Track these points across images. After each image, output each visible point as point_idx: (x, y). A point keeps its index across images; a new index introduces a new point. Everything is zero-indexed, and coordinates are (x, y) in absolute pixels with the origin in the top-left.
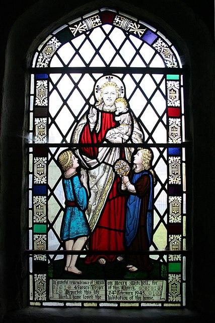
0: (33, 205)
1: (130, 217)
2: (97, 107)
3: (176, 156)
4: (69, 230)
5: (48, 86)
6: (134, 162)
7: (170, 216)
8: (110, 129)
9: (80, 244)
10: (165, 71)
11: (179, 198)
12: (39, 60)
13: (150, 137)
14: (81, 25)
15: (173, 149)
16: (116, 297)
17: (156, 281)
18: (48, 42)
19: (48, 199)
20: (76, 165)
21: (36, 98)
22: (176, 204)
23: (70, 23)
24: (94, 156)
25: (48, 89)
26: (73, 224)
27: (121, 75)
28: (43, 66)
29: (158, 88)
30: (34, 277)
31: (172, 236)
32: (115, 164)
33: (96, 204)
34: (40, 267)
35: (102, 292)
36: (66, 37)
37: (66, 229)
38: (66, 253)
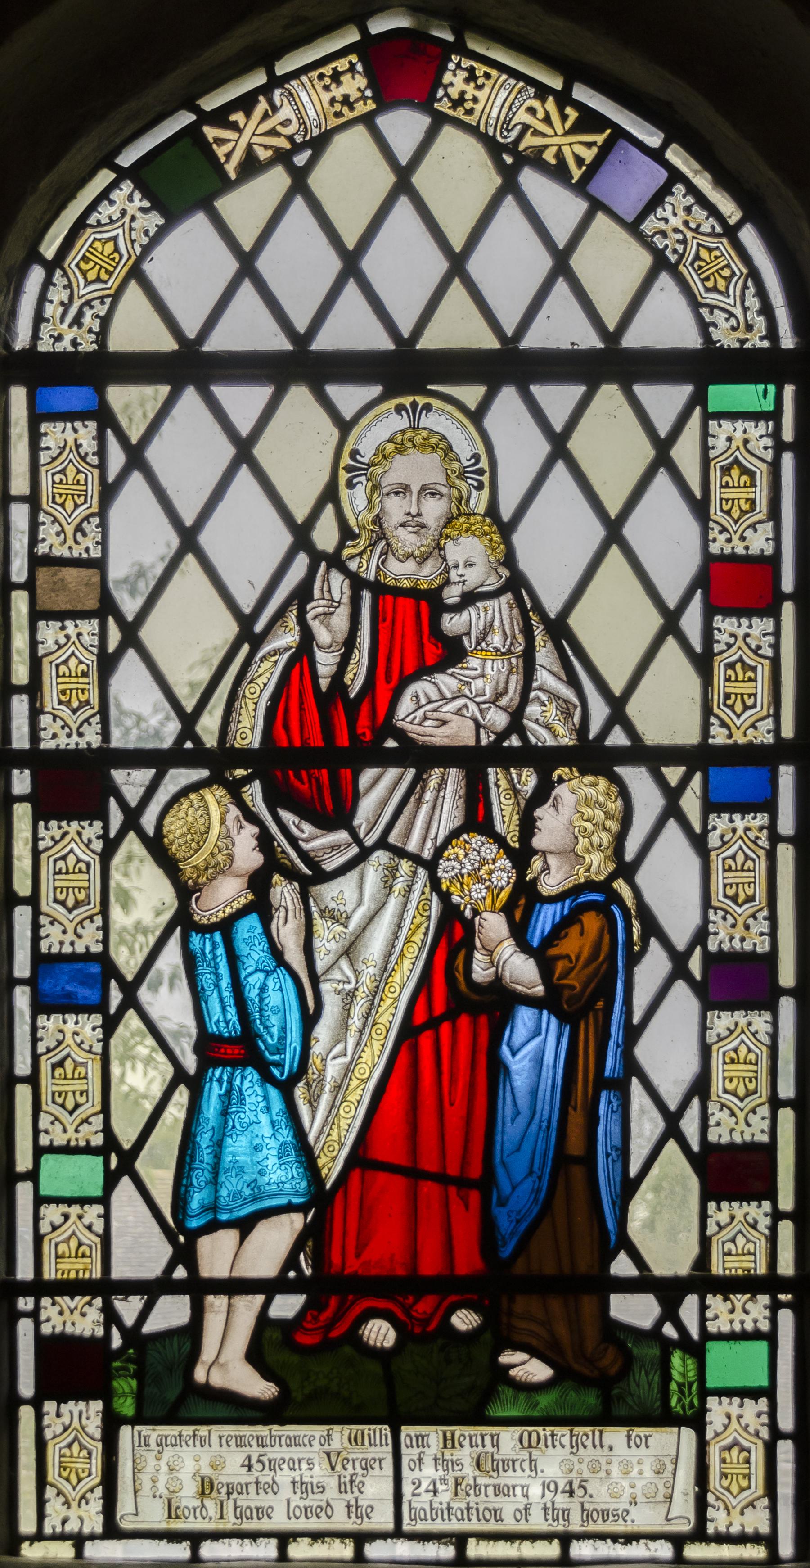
0: (36, 1058)
1: (518, 1113)
2: (353, 566)
3: (745, 808)
4: (215, 1182)
5: (101, 452)
6: (537, 842)
7: (713, 1107)
8: (416, 677)
9: (270, 1247)
10: (705, 366)
11: (760, 1022)
12: (49, 310)
13: (618, 715)
14: (266, 116)
15: (726, 772)
16: (449, 1509)
17: (642, 1431)
18: (92, 207)
19: (110, 1026)
20: (247, 855)
21: (42, 517)
22: (743, 1050)
23: (211, 103)
24: (336, 813)
25: (102, 466)
26: (237, 1147)
27: (471, 394)
28: (74, 343)
29: (663, 458)
30: (39, 1416)
31: (725, 1205)
32: (439, 852)
33: (351, 1064)
34: (72, 1369)
35: (377, 1488)
36: (184, 184)
37: (200, 1176)
38: (199, 1289)
